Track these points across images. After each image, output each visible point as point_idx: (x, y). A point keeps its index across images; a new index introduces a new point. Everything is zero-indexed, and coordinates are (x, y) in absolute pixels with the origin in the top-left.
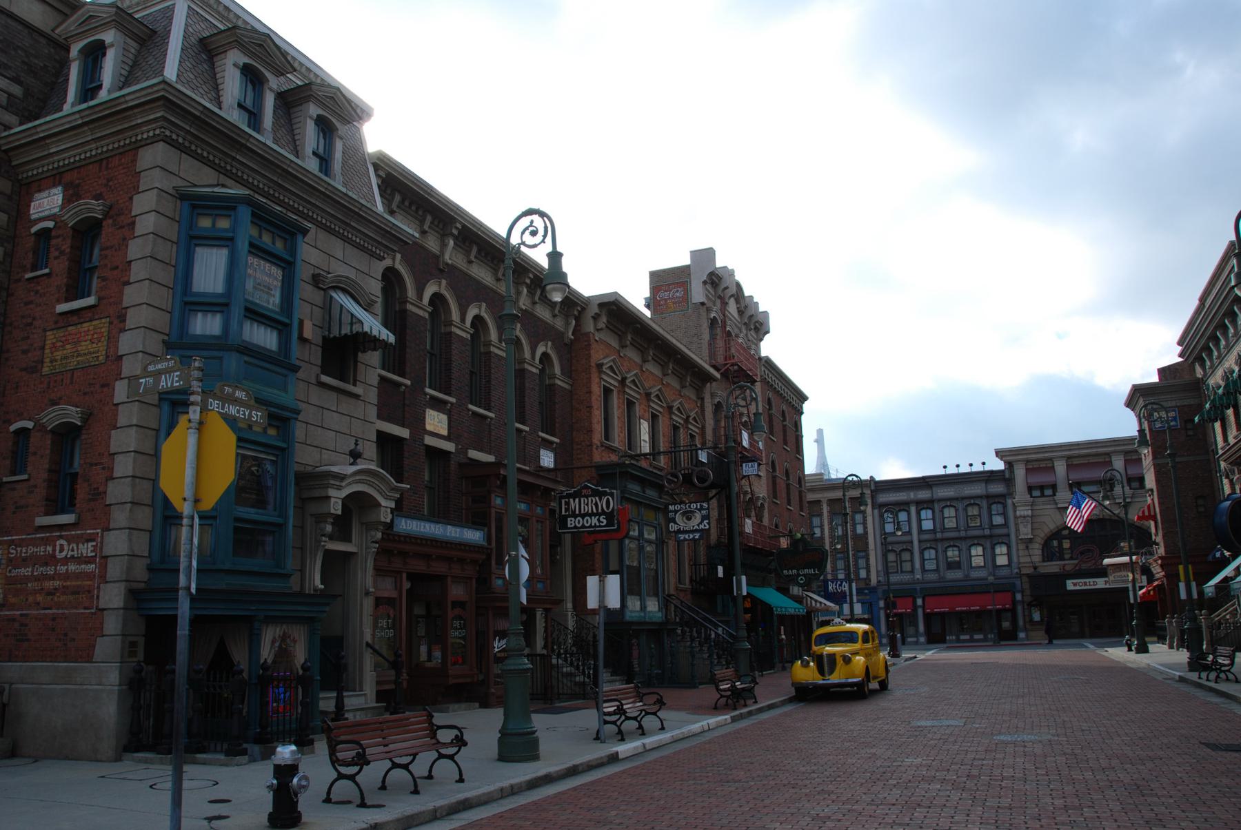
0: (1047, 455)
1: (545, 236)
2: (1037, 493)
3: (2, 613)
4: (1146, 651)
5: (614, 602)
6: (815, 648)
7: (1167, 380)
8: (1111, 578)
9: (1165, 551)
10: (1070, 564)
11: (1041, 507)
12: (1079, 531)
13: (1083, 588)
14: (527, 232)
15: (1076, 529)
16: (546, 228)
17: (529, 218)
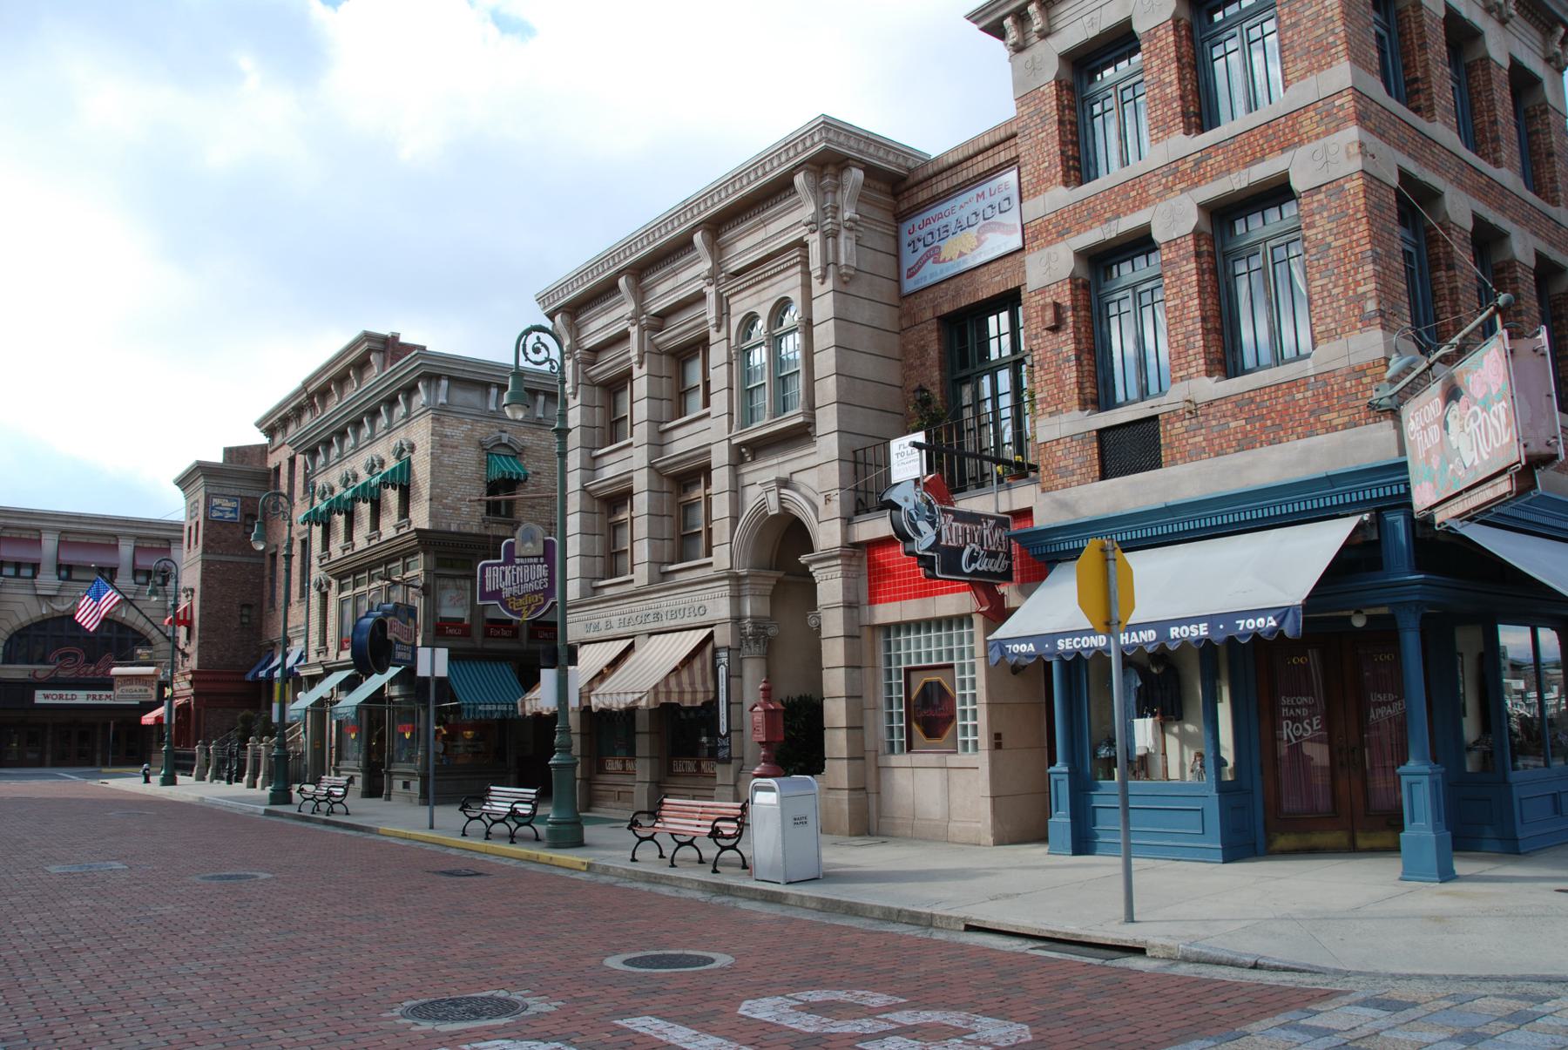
0: (34, 523)
2: (142, 579)
4: (174, 783)
5: (442, 670)
6: (406, 749)
7: (232, 462)
8: (118, 692)
9: (199, 664)
10: (42, 671)
11: (14, 591)
12: (91, 630)
13: (57, 702)
15: (84, 624)
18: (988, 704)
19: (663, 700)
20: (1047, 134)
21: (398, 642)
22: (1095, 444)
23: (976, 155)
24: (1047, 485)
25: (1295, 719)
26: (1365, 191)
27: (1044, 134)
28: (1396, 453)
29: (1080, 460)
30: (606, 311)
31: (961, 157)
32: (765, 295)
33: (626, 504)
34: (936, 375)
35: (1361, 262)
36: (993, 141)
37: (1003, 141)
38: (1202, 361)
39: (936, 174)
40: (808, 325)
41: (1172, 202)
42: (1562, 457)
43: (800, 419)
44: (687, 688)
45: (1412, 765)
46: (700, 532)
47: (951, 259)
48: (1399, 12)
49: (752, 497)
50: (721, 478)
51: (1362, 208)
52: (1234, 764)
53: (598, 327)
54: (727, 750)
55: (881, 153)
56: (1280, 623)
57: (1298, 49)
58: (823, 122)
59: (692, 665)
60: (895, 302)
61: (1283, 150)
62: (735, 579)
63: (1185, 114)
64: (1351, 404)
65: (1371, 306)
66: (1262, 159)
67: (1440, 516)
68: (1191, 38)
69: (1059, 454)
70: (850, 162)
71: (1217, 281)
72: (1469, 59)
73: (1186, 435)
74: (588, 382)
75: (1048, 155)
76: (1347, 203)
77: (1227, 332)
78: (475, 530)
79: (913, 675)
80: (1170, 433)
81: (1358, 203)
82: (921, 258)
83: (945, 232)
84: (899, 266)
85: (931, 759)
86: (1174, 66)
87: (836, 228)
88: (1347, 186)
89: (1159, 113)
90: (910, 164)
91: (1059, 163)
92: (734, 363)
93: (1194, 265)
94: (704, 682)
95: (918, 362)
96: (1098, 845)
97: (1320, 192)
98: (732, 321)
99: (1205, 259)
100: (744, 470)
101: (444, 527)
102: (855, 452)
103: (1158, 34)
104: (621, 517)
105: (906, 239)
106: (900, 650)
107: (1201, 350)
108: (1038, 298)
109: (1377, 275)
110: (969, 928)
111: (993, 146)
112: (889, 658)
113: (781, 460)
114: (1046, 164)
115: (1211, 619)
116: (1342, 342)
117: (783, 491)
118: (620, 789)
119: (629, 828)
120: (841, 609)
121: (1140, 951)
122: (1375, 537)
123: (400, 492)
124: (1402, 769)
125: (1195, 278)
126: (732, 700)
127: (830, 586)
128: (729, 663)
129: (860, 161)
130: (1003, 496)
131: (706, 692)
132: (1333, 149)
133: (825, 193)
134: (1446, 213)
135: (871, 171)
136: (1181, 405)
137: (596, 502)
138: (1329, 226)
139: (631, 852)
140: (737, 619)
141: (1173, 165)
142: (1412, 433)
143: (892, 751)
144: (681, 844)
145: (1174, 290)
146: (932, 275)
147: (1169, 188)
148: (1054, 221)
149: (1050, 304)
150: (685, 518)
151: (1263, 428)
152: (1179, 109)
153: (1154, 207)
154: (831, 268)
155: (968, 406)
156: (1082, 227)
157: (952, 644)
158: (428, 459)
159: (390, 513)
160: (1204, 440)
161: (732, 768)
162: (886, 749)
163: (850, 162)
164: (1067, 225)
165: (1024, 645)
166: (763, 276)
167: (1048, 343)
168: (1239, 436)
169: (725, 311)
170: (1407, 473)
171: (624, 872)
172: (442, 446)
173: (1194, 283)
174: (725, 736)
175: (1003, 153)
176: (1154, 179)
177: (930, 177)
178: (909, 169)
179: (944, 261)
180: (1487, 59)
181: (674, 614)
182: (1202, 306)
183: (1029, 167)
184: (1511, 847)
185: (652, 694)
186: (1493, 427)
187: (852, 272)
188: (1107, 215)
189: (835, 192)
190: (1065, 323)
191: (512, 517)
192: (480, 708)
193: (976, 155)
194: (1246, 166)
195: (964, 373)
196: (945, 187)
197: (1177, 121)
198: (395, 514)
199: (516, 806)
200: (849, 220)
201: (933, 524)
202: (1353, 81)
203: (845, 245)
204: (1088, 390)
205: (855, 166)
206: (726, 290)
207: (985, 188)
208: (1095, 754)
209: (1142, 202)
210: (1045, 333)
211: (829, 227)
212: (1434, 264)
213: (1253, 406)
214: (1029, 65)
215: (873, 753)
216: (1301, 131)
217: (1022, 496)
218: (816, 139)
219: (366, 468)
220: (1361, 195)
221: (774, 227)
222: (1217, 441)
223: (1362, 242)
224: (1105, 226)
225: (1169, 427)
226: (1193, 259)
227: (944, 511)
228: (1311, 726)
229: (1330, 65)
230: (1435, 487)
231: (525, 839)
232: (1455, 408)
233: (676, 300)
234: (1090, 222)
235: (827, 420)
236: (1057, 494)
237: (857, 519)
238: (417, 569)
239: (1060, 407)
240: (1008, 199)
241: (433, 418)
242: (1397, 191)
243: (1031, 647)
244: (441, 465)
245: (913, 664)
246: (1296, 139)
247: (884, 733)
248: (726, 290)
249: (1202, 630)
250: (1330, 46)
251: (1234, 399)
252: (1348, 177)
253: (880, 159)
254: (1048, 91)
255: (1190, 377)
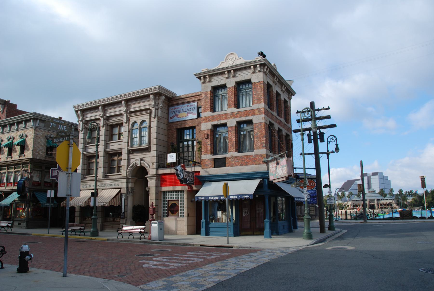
1: (335, 140)
3: (1, 172)
14: (331, 139)
16: (335, 139)
17: (331, 137)
18: (187, 208)
19: (111, 205)
20: (208, 101)
21: (27, 187)
22: (213, 161)
23: (188, 97)
24: (203, 167)
25: (246, 212)
26: (265, 126)
27: (207, 101)
28: (266, 170)
29: (210, 164)
30: (93, 113)
31: (185, 97)
32: (139, 118)
33: (94, 158)
34: (175, 140)
35: (263, 137)
36: (192, 96)
37: (194, 96)
38: (235, 149)
39: (179, 99)
40: (150, 127)
41: (231, 120)
42: (293, 176)
43: (147, 147)
44: (116, 202)
45: (266, 220)
46: (116, 167)
47: (181, 117)
48: (269, 91)
49: (133, 161)
50: (124, 156)
51: (264, 128)
52: (235, 220)
53: (90, 116)
54: (124, 216)
55: (168, 93)
56: (249, 197)
57: (256, 99)
58: (159, 87)
59: (116, 197)
60: (167, 124)
61: (252, 115)
62: (128, 179)
63: (235, 104)
64: (260, 160)
65: (264, 145)
66: (248, 116)
67: (274, 181)
68: (237, 90)
69: (206, 162)
70: (163, 95)
71: (238, 135)
72: (278, 98)
73: (231, 162)
74: (85, 128)
75: (208, 105)
76: (262, 127)
77: (239, 144)
78: (43, 159)
79: (169, 201)
80: (228, 161)
81: (263, 127)
82: (174, 115)
83: (180, 111)
84: (168, 116)
85: (173, 218)
86: (234, 95)
87: (158, 108)
88: (262, 124)
89: (230, 103)
90: (173, 96)
91: (210, 107)
92: (130, 132)
93: (234, 132)
94: (119, 201)
95: (171, 137)
96: (210, 234)
97: (257, 124)
98: (130, 122)
99: (236, 131)
100: (130, 155)
101: (35, 157)
102: (159, 155)
103: (231, 88)
104: (92, 161)
105: (170, 111)
106: (167, 196)
107: (235, 147)
108: (203, 132)
109: (265, 140)
110: (201, 246)
111: (192, 97)
112: (164, 198)
113: (140, 154)
114: (207, 107)
115: (238, 195)
116: (259, 150)
117: (141, 161)
118: (90, 224)
119: (117, 231)
120: (155, 187)
121: (232, 247)
122: (262, 183)
123: (20, 147)
124: (265, 221)
125: (234, 134)
126: (125, 205)
127: (152, 183)
128: (125, 197)
129: (164, 94)
130: (193, 168)
131: (119, 203)
132: (260, 117)
133: (156, 100)
134: (274, 128)
135: (166, 96)
136: (230, 156)
137: (86, 157)
138: (258, 130)
139: (117, 237)
140: (127, 187)
141: (232, 113)
142: (270, 168)
143: (164, 216)
144: (130, 235)
145: (230, 136)
146: (176, 120)
147: (231, 117)
148: (208, 118)
149: (206, 134)
150: (111, 163)
151: (245, 163)
152: (234, 103)
153: (228, 120)
154: (157, 116)
155: (181, 147)
156: (214, 121)
157: (171, 196)
158: (33, 140)
159: (16, 152)
160: (234, 163)
161: (125, 220)
162: (163, 216)
163: (163, 95)
164: (210, 119)
165: (202, 198)
166: (139, 114)
167: (205, 141)
168: (240, 163)
169: (128, 119)
170: (269, 173)
171: (118, 240)
172: (36, 137)
173: (234, 135)
174: (123, 213)
175: (194, 98)
176: (228, 115)
177: (177, 99)
178: (173, 97)
179: (179, 117)
180: (281, 99)
181: (110, 185)
182: (235, 139)
183: (203, 106)
184: (278, 234)
185: (109, 203)
186: (284, 170)
187: (160, 117)
188: (219, 119)
189: (158, 100)
190: (209, 138)
191: (52, 156)
192: (46, 204)
193: (188, 97)
194: (245, 116)
195: (181, 141)
196: (181, 102)
197: (233, 105)
198: (18, 153)
199: (81, 228)
200: (161, 107)
201: (183, 174)
202: (264, 107)
203: (160, 111)
204: (212, 151)
205: (163, 95)
206: (129, 115)
207: (190, 104)
208: (210, 218)
209: (225, 118)
210: (204, 139)
211: (157, 107)
212: (272, 136)
213: (243, 158)
214: (205, 86)
215: (160, 217)
216: (255, 113)
217: (197, 169)
218: (157, 89)
219: (7, 139)
220: (264, 126)
221: (142, 104)
222: (236, 164)
223: (264, 134)
224: (218, 121)
225: (228, 160)
226: (234, 131)
227: (185, 171)
228: (248, 213)
229: (261, 103)
230: (274, 177)
231: (82, 235)
232: (278, 166)
233: (114, 114)
234: (215, 120)
235: (154, 148)
236: (205, 169)
237: (159, 169)
238: (29, 168)
239: (207, 153)
240: (194, 108)
241: (34, 130)
242: (269, 125)
243: (204, 198)
244: (36, 142)
245: (170, 199)
246: (254, 114)
247: (162, 213)
248: (129, 115)
249: (236, 197)
250: (261, 100)
251: (240, 157)
252: (262, 123)
253: (168, 94)
254: (208, 93)
255: (232, 152)
